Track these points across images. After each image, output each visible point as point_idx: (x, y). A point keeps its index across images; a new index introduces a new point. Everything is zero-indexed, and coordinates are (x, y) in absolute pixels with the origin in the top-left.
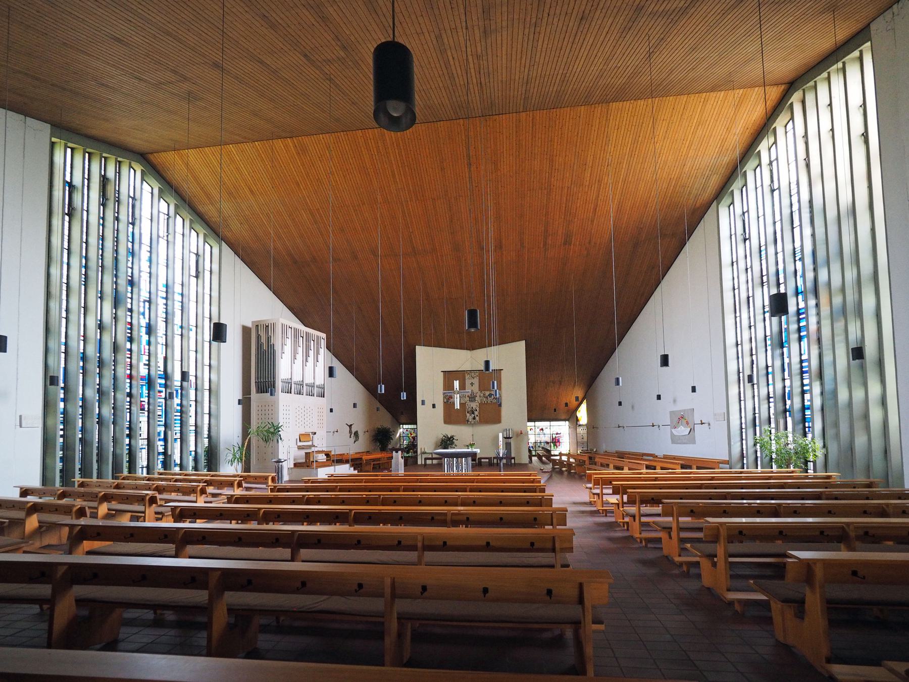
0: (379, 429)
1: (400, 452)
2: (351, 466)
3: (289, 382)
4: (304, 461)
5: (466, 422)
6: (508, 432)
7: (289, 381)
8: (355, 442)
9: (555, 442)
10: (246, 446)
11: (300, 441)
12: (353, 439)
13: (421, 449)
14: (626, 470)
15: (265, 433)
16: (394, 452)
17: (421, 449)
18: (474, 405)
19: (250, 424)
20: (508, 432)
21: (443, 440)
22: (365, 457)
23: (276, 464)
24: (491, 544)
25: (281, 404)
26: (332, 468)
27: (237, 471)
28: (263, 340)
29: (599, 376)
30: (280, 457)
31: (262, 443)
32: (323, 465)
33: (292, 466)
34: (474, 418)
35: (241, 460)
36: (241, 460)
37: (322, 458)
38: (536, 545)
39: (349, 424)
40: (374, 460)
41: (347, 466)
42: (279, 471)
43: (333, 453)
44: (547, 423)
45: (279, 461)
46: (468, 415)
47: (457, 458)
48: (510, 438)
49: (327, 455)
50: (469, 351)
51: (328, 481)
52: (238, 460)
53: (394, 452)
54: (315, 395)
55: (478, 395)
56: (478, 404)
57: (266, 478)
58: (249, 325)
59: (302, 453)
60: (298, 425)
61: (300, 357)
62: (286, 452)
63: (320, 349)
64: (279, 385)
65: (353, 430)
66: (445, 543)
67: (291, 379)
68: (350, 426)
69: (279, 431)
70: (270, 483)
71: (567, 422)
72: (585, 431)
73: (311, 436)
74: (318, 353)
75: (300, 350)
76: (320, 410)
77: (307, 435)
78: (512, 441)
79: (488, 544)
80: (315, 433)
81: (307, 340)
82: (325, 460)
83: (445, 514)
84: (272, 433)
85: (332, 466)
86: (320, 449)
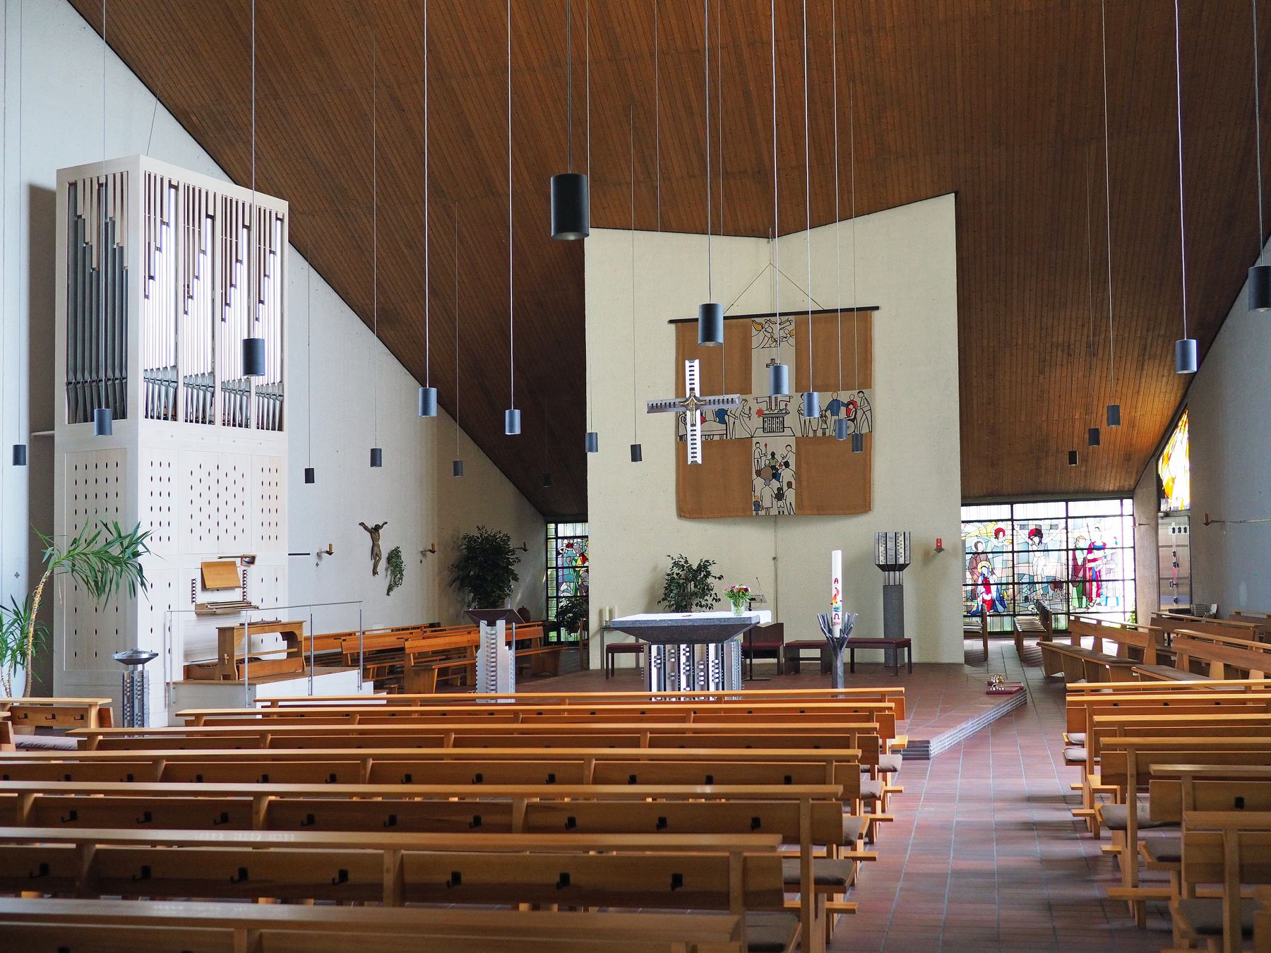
0: (471, 539)
1: (501, 624)
2: (365, 677)
3: (165, 381)
4: (213, 658)
5: (750, 510)
6: (891, 544)
7: (170, 375)
8: (390, 589)
9: (1084, 581)
10: (36, 606)
11: (204, 588)
12: (383, 579)
13: (601, 613)
14: (1257, 679)
15: (94, 560)
16: (483, 624)
17: (601, 613)
18: (781, 445)
19: (51, 533)
20: (891, 544)
21: (671, 581)
22: (414, 645)
23: (125, 670)
24: (572, 879)
25: (145, 454)
26: (303, 681)
27: (9, 694)
28: (91, 235)
29: (1228, 321)
30: (140, 648)
31: (88, 599)
32: (277, 672)
33: (179, 676)
34: (780, 495)
35: (24, 655)
36: (24, 655)
37: (273, 646)
38: (689, 884)
39: (371, 525)
40: (446, 654)
41: (353, 675)
42: (133, 694)
43: (306, 632)
44: (1057, 508)
45: (134, 660)
46: (758, 482)
47: (691, 643)
48: (901, 567)
49: (290, 637)
50: (764, 241)
51: (267, 718)
52: (14, 657)
53: (483, 624)
54: (253, 422)
55: (792, 408)
56: (792, 441)
57: (82, 714)
58: (49, 181)
59: (209, 630)
60: (198, 531)
61: (202, 288)
62: (158, 631)
63: (270, 258)
64: (138, 392)
65: (385, 548)
66: (456, 877)
67: (175, 367)
68: (375, 531)
69: (136, 554)
70: (93, 726)
71: (1128, 503)
72: (1184, 538)
73: (240, 570)
74: (262, 273)
75: (205, 262)
76: (266, 477)
77: (225, 565)
78: (906, 578)
79: (565, 879)
80: (252, 560)
81: (229, 229)
82: (284, 656)
83: (723, 865)
84: (117, 561)
85: (302, 675)
86: (269, 617)
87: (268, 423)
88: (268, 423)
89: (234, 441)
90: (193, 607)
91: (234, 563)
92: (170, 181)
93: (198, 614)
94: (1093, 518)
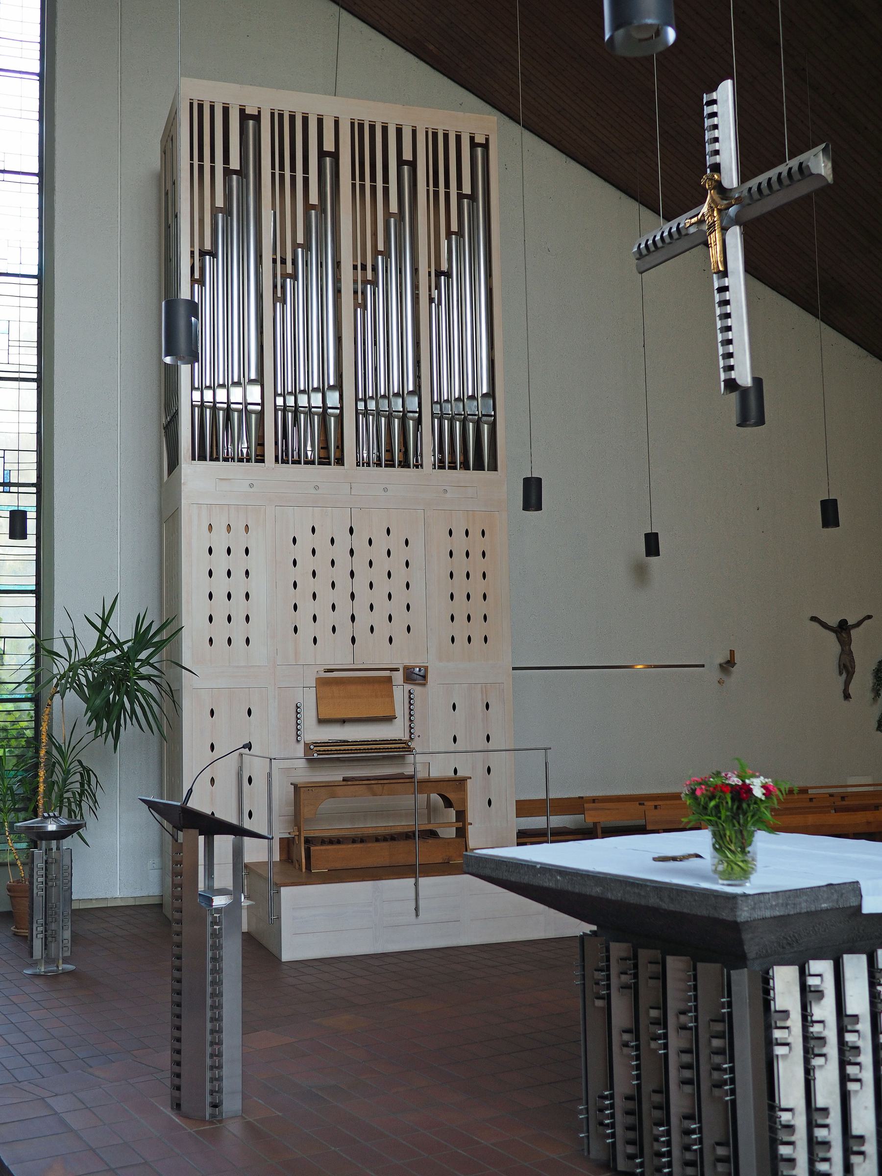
87: (390, 450)
88: (390, 450)
89: (385, 490)
90: (300, 750)
91: (389, 680)
92: (472, 139)
93: (310, 761)
94: (10, 272)
